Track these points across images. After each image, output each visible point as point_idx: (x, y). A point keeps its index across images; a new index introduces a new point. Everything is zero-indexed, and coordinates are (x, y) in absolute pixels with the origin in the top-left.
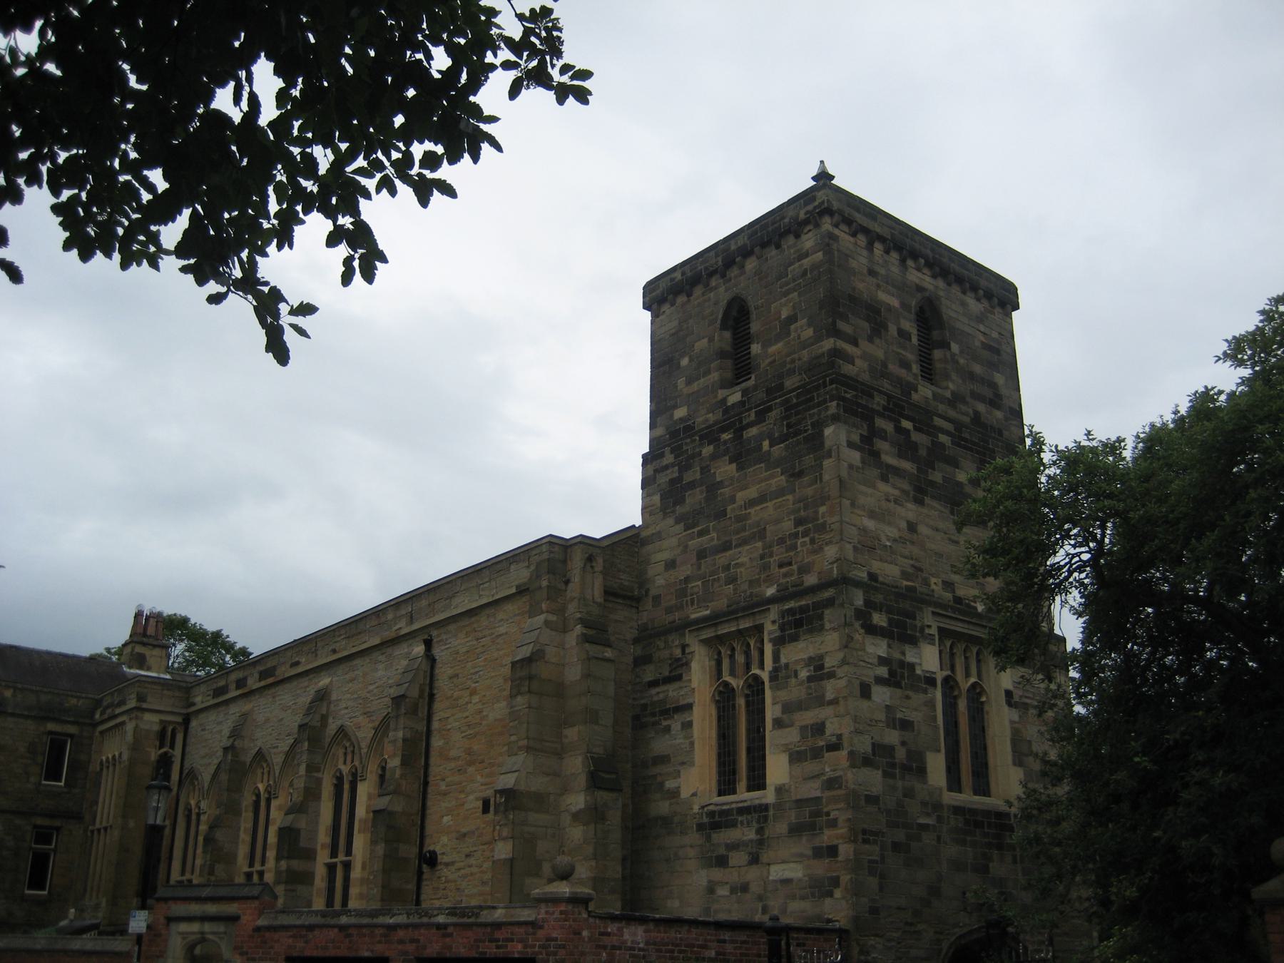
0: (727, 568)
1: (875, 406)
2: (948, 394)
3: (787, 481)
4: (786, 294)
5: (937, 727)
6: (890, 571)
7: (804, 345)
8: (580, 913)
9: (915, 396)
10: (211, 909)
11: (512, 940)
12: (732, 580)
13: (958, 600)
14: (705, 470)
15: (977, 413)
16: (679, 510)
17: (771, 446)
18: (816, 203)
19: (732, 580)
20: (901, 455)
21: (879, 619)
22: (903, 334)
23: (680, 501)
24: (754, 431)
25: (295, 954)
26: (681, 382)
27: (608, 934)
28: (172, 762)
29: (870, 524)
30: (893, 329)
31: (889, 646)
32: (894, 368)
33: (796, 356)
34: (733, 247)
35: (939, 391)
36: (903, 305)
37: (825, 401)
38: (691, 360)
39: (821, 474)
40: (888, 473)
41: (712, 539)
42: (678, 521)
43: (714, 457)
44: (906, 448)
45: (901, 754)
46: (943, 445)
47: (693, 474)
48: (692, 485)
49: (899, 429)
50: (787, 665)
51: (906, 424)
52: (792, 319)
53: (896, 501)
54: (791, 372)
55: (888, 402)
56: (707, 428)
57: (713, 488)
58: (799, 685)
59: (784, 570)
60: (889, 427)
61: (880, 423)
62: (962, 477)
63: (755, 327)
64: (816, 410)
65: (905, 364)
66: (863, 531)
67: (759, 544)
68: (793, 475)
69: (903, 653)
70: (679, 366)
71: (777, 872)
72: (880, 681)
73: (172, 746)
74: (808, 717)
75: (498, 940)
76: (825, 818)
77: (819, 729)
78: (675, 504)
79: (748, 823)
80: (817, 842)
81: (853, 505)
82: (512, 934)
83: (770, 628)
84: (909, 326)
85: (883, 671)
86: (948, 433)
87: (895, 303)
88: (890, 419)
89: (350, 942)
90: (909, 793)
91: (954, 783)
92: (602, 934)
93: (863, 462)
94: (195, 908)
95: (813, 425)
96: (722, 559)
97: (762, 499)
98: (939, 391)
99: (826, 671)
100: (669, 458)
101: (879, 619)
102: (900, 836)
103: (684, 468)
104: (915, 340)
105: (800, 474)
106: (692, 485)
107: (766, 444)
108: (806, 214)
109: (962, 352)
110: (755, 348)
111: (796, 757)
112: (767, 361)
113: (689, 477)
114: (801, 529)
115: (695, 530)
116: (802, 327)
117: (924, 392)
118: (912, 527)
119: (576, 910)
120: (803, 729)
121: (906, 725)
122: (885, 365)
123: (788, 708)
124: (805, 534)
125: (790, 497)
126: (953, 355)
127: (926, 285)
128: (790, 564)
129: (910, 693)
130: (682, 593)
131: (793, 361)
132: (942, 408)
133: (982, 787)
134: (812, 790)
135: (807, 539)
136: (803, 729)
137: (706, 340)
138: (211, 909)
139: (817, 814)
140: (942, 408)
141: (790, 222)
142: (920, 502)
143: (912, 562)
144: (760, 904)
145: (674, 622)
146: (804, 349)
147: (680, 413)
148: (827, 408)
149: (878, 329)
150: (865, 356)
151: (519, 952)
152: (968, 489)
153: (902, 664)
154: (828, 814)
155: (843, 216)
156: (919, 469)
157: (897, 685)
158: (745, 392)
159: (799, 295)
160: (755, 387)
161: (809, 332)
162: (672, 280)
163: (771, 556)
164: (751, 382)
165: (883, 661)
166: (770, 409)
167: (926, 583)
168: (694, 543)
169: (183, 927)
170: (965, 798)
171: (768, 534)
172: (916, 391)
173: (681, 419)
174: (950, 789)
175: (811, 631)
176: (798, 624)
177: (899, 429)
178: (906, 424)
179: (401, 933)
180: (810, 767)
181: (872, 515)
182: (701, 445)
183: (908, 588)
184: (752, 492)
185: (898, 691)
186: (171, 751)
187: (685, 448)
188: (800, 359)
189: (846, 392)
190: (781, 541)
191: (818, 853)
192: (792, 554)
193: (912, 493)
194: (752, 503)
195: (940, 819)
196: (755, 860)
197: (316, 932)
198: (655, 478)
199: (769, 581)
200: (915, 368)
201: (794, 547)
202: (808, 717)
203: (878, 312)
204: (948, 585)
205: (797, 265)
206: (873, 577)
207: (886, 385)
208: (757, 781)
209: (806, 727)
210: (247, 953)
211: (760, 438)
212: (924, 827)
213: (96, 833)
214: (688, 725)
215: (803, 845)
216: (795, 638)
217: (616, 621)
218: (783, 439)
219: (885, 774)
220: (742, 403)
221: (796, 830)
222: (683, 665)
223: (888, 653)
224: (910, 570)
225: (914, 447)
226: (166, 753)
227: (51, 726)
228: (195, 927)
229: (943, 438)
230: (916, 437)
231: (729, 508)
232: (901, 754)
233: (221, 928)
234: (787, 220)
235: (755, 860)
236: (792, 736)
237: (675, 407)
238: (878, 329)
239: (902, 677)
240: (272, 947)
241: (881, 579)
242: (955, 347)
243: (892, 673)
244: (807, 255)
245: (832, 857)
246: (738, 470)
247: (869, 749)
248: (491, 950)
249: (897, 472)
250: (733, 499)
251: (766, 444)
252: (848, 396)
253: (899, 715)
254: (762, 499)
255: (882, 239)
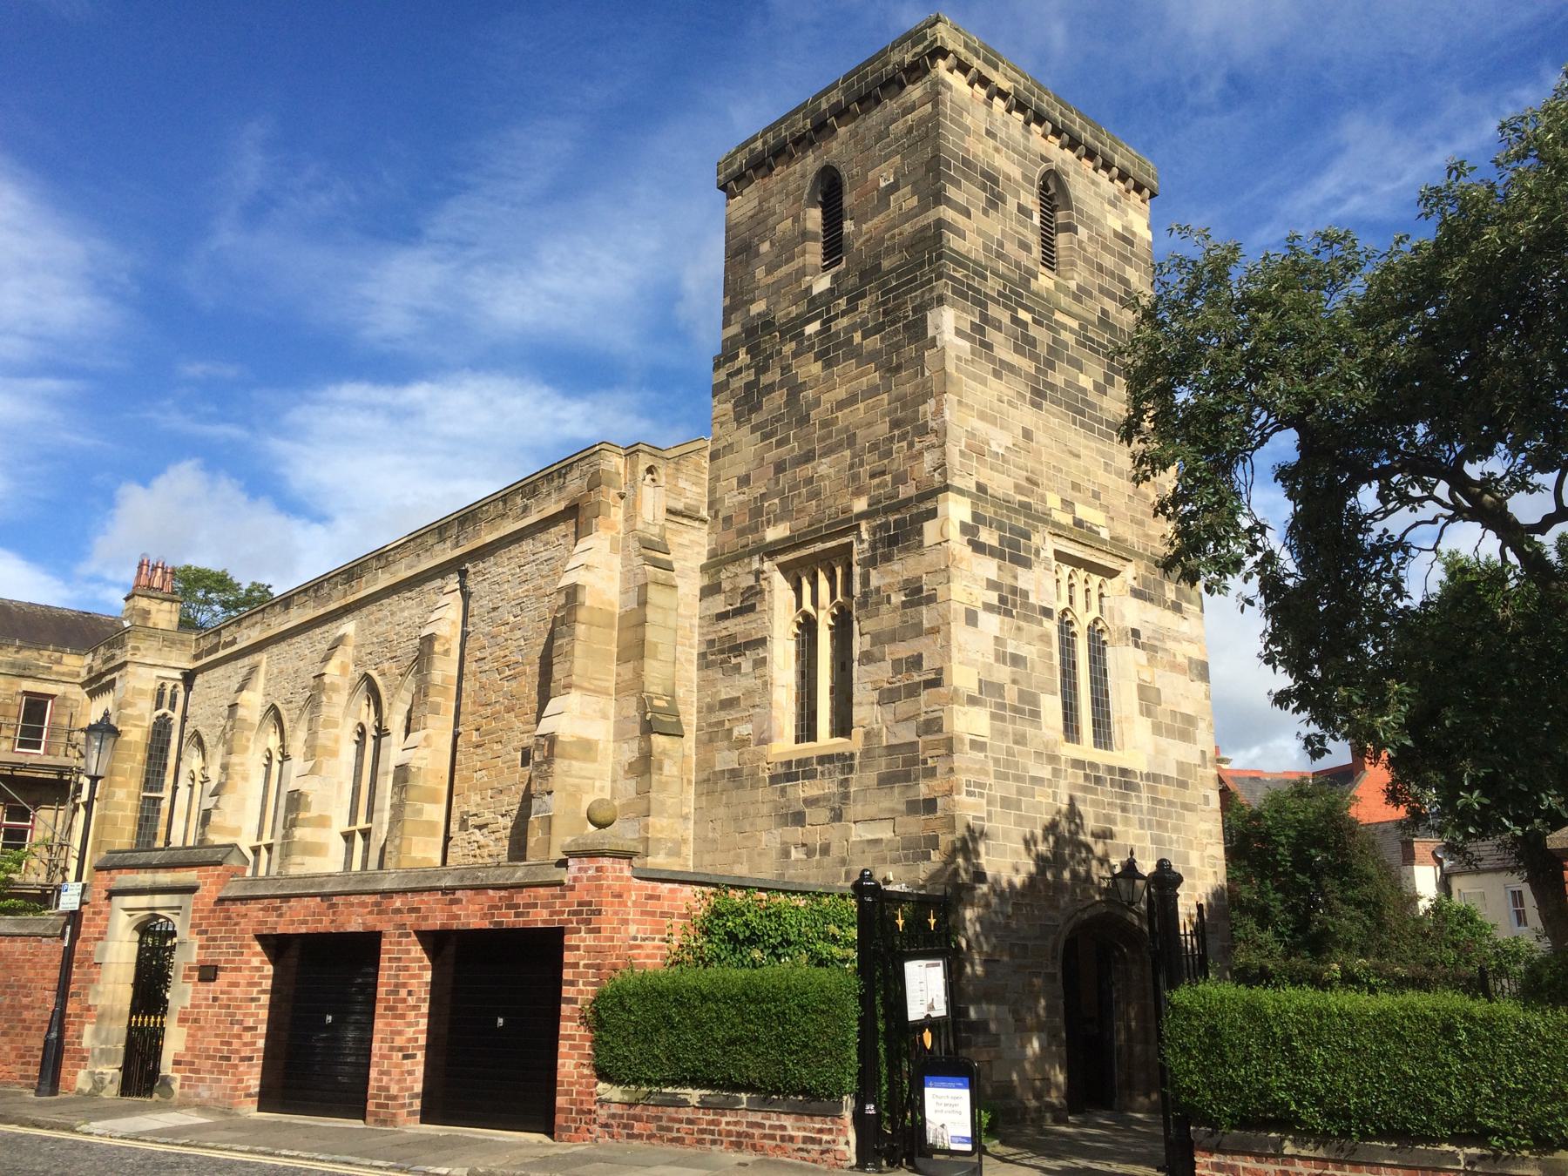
0: (809, 481)
1: (988, 291)
2: (1073, 285)
3: (882, 378)
4: (887, 158)
5: (1051, 668)
6: (1001, 485)
7: (908, 216)
8: (621, 870)
9: (1034, 285)
10: (165, 878)
11: (535, 905)
12: (815, 495)
13: (1079, 523)
14: (786, 369)
15: (1104, 312)
16: (755, 418)
17: (864, 338)
18: (926, 43)
19: (815, 495)
20: (1018, 350)
21: (988, 536)
22: (1022, 209)
23: (757, 408)
24: (843, 322)
25: (265, 932)
26: (760, 273)
27: (658, 898)
28: (171, 727)
29: (981, 427)
30: (1011, 204)
31: (1000, 568)
32: (1011, 249)
33: (896, 231)
34: (824, 106)
35: (1062, 281)
36: (1025, 177)
37: (930, 281)
38: (772, 244)
39: (923, 368)
40: (1002, 369)
41: (793, 449)
42: (754, 430)
43: (795, 355)
44: (1025, 344)
45: (1011, 695)
46: (1065, 345)
47: (773, 376)
48: (770, 388)
49: (1015, 320)
50: (878, 590)
51: (1024, 315)
52: (893, 188)
53: (1010, 403)
54: (890, 251)
55: (1005, 287)
56: (788, 322)
57: (795, 390)
58: (894, 611)
59: (876, 481)
60: (1005, 318)
61: (994, 311)
62: (1085, 381)
63: (849, 200)
64: (918, 292)
65: (1025, 246)
66: (971, 434)
67: (848, 453)
68: (889, 370)
69: (1015, 577)
70: (757, 254)
71: (860, 833)
72: (988, 607)
73: (172, 706)
74: (903, 650)
75: (517, 906)
76: (921, 766)
77: (916, 662)
78: (751, 411)
79: (830, 773)
80: (911, 795)
81: (960, 402)
82: (535, 898)
83: (859, 551)
84: (1031, 200)
85: (993, 597)
86: (1072, 331)
87: (1016, 173)
88: (1006, 306)
89: (334, 913)
90: (1020, 740)
91: (1071, 729)
92: (650, 897)
93: (973, 353)
94: (144, 878)
95: (915, 310)
96: (807, 470)
97: (852, 400)
98: (1062, 281)
99: (925, 594)
100: (743, 357)
101: (988, 536)
102: (1010, 789)
103: (762, 370)
104: (1036, 220)
105: (899, 368)
106: (770, 388)
107: (857, 338)
108: (914, 56)
109: (1090, 238)
110: (848, 226)
111: (888, 697)
112: (861, 241)
113: (765, 380)
114: (896, 432)
115: (774, 440)
116: (904, 196)
117: (1044, 281)
118: (1027, 434)
119: (618, 866)
120: (897, 663)
121: (1017, 660)
122: (1001, 245)
123: (878, 639)
124: (903, 437)
125: (885, 396)
126: (1080, 242)
127: (1052, 156)
128: (883, 473)
129: (1022, 623)
130: (756, 512)
131: (893, 237)
132: (1065, 301)
133: (1103, 735)
134: (907, 734)
135: (904, 444)
136: (897, 663)
137: (790, 221)
138: (165, 878)
139: (913, 761)
140: (1065, 301)
141: (894, 68)
142: (1038, 406)
143: (1025, 473)
144: (844, 869)
145: (747, 545)
146: (907, 221)
147: (758, 307)
148: (932, 289)
149: (995, 201)
150: (980, 233)
151: (544, 921)
152: (1093, 397)
153: (1014, 591)
154: (925, 762)
155: (959, 59)
156: (1037, 369)
157: (1008, 613)
158: (835, 278)
159: (903, 158)
160: (847, 272)
161: (914, 201)
162: (752, 151)
163: (862, 465)
164: (843, 265)
165: (992, 585)
166: (863, 295)
167: (1043, 500)
168: (773, 455)
169: (130, 901)
170: (1086, 748)
171: (859, 440)
172: (1036, 278)
173: (759, 314)
174: (1068, 739)
175: (907, 549)
176: (892, 541)
177: (1015, 320)
178: (1024, 315)
179: (398, 902)
180: (903, 707)
181: (982, 416)
182: (783, 341)
183: (1022, 504)
184: (841, 393)
185: (1007, 619)
186: (170, 712)
187: (763, 346)
188: (901, 234)
189: (955, 270)
190: (874, 447)
191: (914, 807)
192: (886, 461)
193: (1028, 395)
194: (841, 405)
195: (1056, 772)
196: (837, 816)
197: (293, 902)
198: (728, 383)
199: (858, 493)
200: (1037, 252)
201: (888, 454)
202: (903, 650)
203: (995, 181)
204: (1067, 505)
205: (901, 121)
206: (981, 488)
207: (1001, 267)
208: (842, 725)
209: (900, 660)
210: (206, 932)
211: (852, 328)
212: (1036, 780)
213: (264, 852)
214: (761, 663)
215: (895, 799)
216: (888, 558)
217: (680, 545)
218: (878, 329)
219: (993, 716)
220: (831, 290)
221: (886, 780)
222: (757, 593)
223: (999, 576)
224: (1024, 483)
225: (1032, 342)
226: (165, 715)
227: (28, 685)
228: (143, 901)
229: (1065, 336)
230: (1034, 331)
231: (812, 413)
232: (1011, 695)
233: (173, 900)
234: (890, 67)
235: (837, 816)
236: (882, 672)
237: (752, 301)
238: (995, 201)
239: (1015, 606)
240: (237, 924)
241: (989, 491)
242: (1083, 233)
243: (1002, 600)
244: (913, 108)
245: (929, 813)
246: (824, 368)
247: (975, 686)
248: (509, 919)
249: (1011, 368)
250: (817, 403)
251: (857, 338)
252: (957, 275)
253: (1009, 650)
254: (852, 400)
255: (1003, 95)
